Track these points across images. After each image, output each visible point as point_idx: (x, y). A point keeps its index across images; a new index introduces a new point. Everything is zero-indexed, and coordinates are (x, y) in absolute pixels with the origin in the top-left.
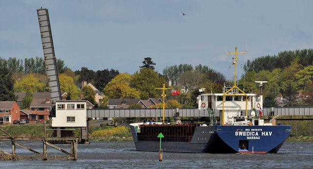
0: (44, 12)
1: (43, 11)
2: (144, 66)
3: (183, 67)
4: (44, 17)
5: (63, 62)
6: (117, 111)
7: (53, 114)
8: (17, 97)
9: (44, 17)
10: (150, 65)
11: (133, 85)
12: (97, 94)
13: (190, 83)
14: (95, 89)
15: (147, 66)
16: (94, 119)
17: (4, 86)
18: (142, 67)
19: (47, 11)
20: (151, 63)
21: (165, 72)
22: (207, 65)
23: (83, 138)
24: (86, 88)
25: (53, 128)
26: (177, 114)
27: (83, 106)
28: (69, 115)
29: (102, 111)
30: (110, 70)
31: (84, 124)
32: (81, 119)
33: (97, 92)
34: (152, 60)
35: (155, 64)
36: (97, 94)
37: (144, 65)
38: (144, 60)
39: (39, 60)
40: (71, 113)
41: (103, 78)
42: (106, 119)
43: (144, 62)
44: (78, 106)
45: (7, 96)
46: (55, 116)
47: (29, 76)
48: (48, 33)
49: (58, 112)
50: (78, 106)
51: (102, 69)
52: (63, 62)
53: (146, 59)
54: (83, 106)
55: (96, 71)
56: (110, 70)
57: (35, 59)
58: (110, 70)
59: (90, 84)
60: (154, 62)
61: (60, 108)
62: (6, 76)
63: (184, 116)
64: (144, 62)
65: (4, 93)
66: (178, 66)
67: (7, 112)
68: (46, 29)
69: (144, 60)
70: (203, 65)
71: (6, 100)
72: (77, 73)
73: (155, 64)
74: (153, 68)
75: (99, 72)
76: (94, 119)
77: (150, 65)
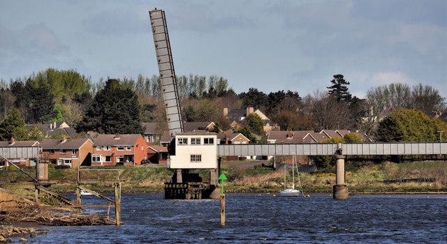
0: (159, 14)
1: (158, 13)
3: (395, 88)
4: (159, 22)
6: (279, 147)
7: (172, 151)
8: (145, 128)
9: (159, 22)
10: (342, 85)
11: (132, 102)
12: (268, 125)
14: (264, 117)
16: (249, 158)
18: (330, 88)
19: (163, 12)
20: (343, 82)
21: (369, 96)
22: (430, 85)
23: (212, 184)
24: (251, 116)
25: (172, 170)
26: (339, 152)
27: (212, 141)
28: (194, 153)
29: (258, 147)
30: (286, 92)
31: (214, 165)
32: (209, 157)
33: (266, 122)
35: (349, 83)
36: (268, 125)
38: (333, 78)
39: (193, 79)
40: (195, 150)
41: (274, 102)
42: (265, 158)
43: (333, 81)
44: (206, 141)
45: (131, 127)
46: (173, 153)
48: (165, 43)
49: (178, 148)
50: (206, 141)
51: (275, 91)
54: (212, 141)
56: (286, 92)
57: (188, 77)
59: (258, 112)
60: (347, 81)
61: (181, 143)
62: (130, 100)
63: (349, 153)
64: (333, 81)
66: (388, 87)
67: (129, 149)
68: (162, 37)
69: (333, 78)
71: (129, 132)
72: (242, 95)
73: (349, 83)
74: (345, 89)
75: (271, 95)
76: (249, 158)
77: (342, 85)
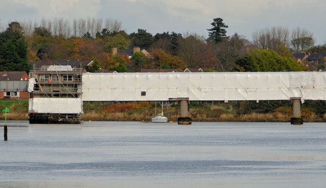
2: (212, 30)
5: (236, 35)
10: (221, 28)
13: (269, 47)
15: (217, 29)
17: (16, 53)
20: (223, 25)
34: (223, 22)
35: (227, 27)
37: (213, 27)
38: (213, 21)
43: (213, 24)
47: (16, 31)
52: (236, 35)
53: (215, 20)
55: (154, 35)
58: (170, 33)
62: (18, 41)
64: (213, 24)
65: (16, 62)
70: (64, 20)
73: (227, 27)
74: (224, 32)
77: (221, 28)
